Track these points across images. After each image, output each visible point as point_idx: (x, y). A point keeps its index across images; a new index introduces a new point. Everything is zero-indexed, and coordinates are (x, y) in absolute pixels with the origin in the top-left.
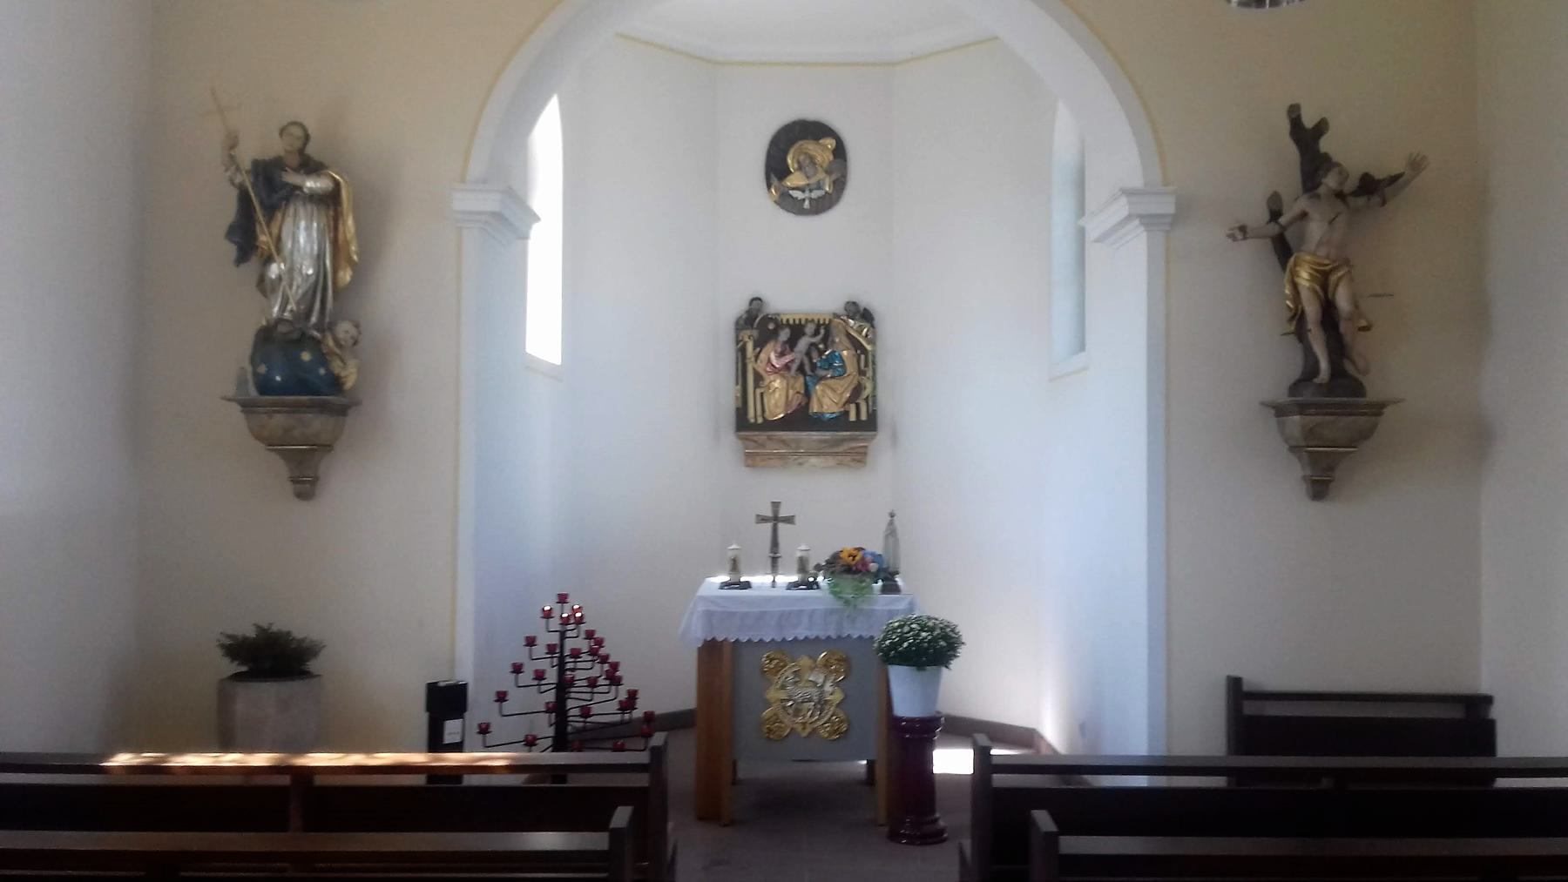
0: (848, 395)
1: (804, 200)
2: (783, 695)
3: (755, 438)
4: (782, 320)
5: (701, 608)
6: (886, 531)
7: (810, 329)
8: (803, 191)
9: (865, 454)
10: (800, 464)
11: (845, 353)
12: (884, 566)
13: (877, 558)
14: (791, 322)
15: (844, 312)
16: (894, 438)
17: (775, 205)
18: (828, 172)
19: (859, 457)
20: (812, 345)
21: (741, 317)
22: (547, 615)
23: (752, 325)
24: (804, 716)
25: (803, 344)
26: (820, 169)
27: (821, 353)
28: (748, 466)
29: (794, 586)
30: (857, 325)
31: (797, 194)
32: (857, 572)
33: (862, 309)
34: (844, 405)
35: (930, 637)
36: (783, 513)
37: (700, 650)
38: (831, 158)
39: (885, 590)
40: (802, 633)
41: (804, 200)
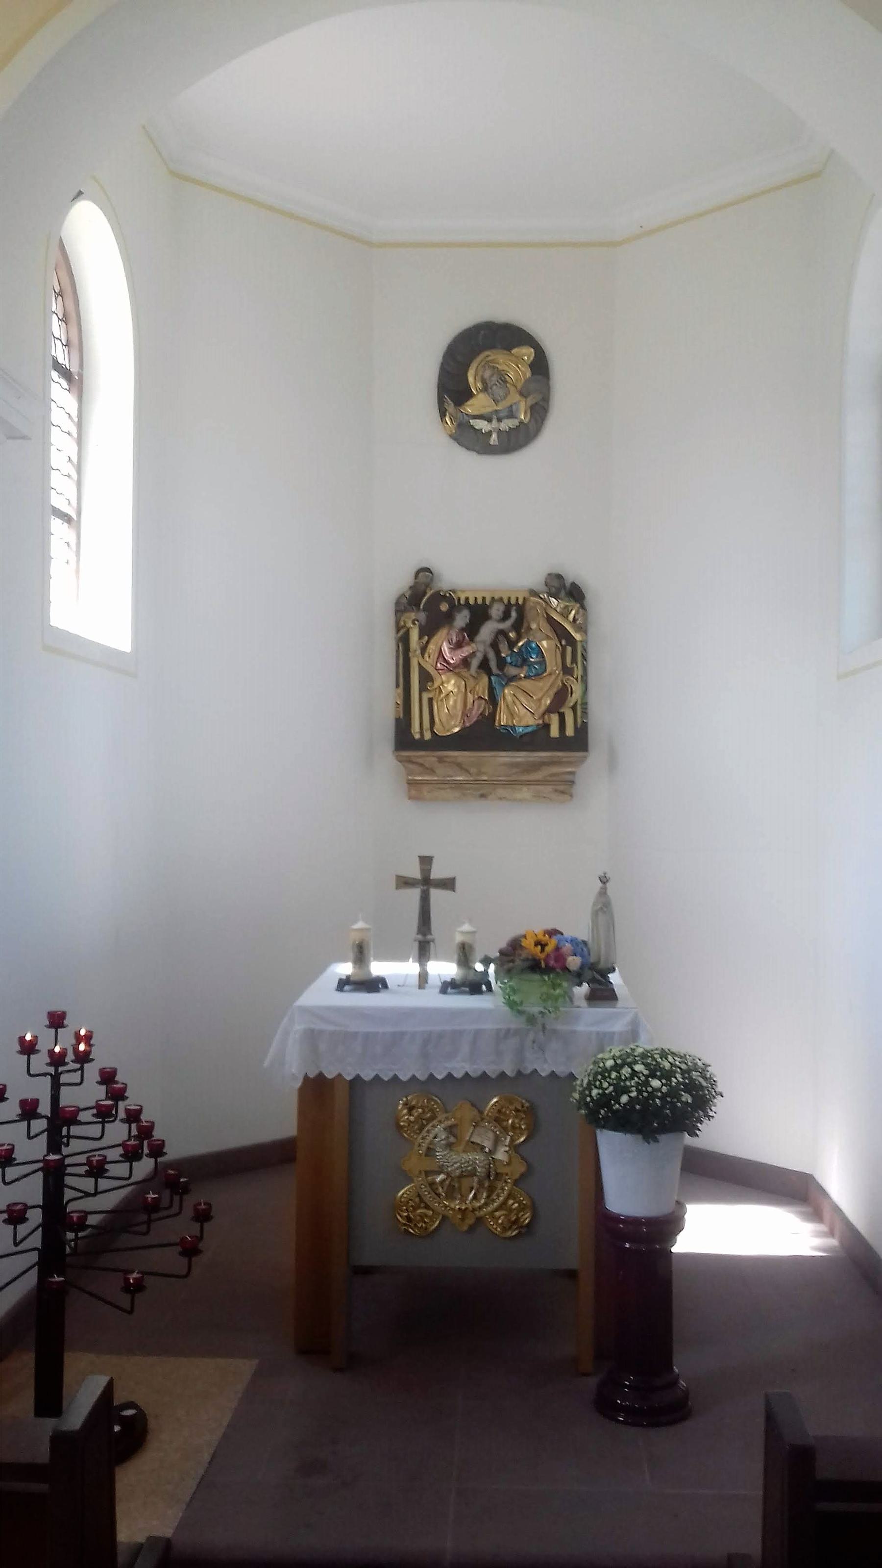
0: (548, 702)
1: (489, 434)
2: (428, 1165)
3: (420, 760)
4: (459, 599)
5: (299, 1027)
6: (594, 905)
7: (496, 611)
8: (489, 420)
9: (572, 782)
10: (483, 796)
11: (545, 643)
12: (592, 959)
13: (580, 946)
14: (472, 602)
15: (545, 589)
16: (612, 764)
17: (452, 441)
18: (523, 394)
19: (561, 788)
20: (502, 633)
21: (404, 595)
22: (28, 1049)
23: (418, 605)
24: (463, 1199)
25: (487, 631)
26: (512, 389)
27: (512, 644)
28: (410, 798)
29: (448, 987)
30: (562, 606)
31: (482, 425)
32: (548, 970)
33: (568, 584)
34: (544, 714)
35: (664, 1089)
36: (415, 872)
37: (301, 1090)
38: (529, 374)
39: (593, 998)
40: (460, 1067)
41: (489, 434)
